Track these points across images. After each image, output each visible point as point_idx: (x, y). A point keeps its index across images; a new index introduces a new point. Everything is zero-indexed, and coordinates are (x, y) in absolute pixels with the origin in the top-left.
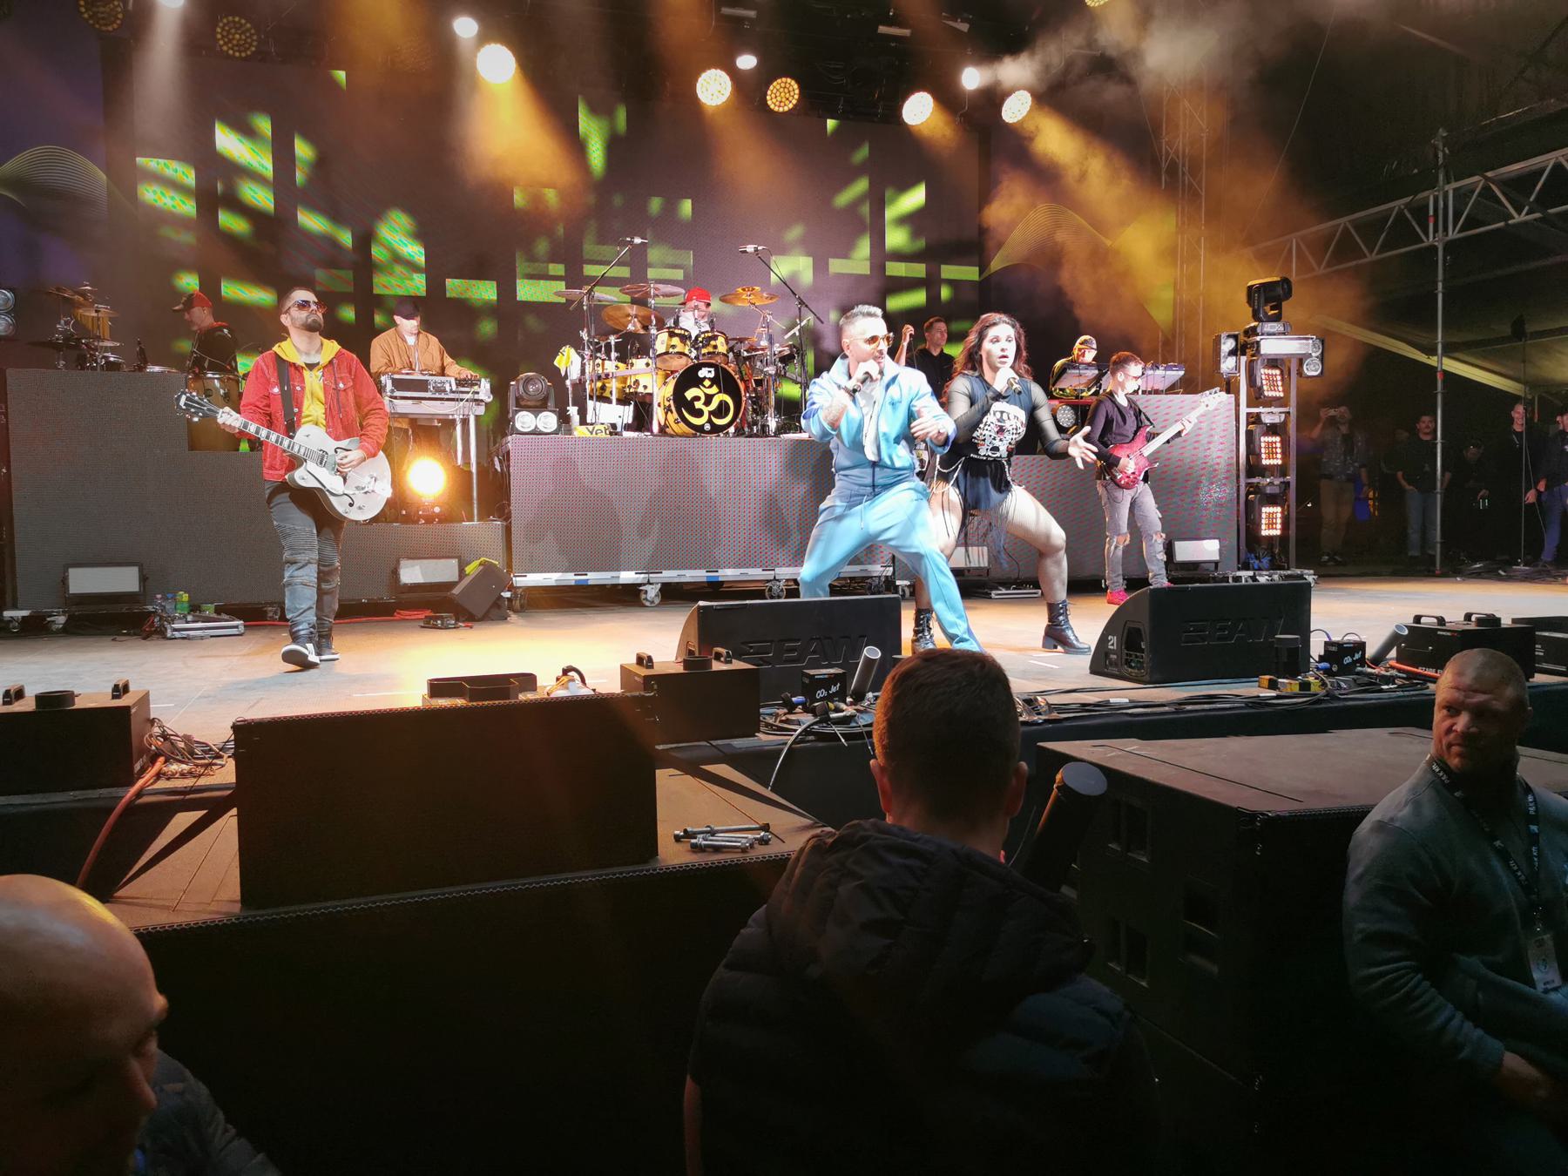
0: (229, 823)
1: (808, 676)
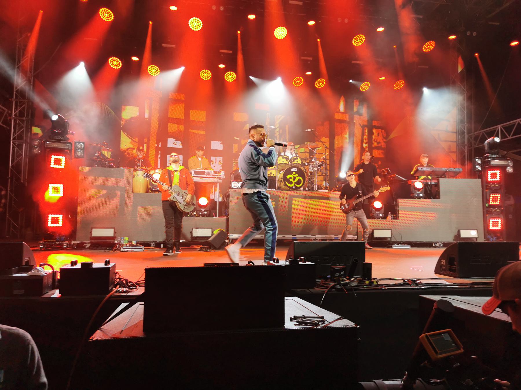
0: (139, 308)
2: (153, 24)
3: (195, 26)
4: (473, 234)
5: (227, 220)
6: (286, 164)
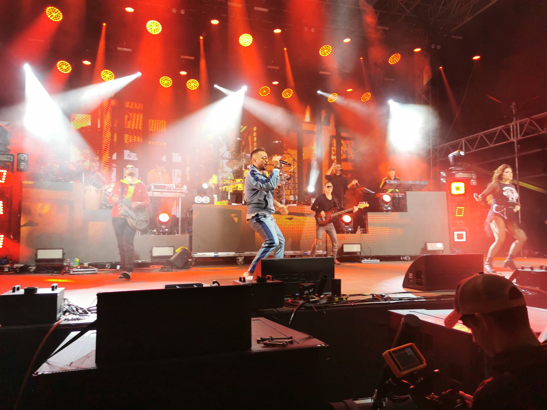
0: (91, 335)
1: (301, 285)
2: (107, 26)
3: (153, 29)
5: (191, 238)
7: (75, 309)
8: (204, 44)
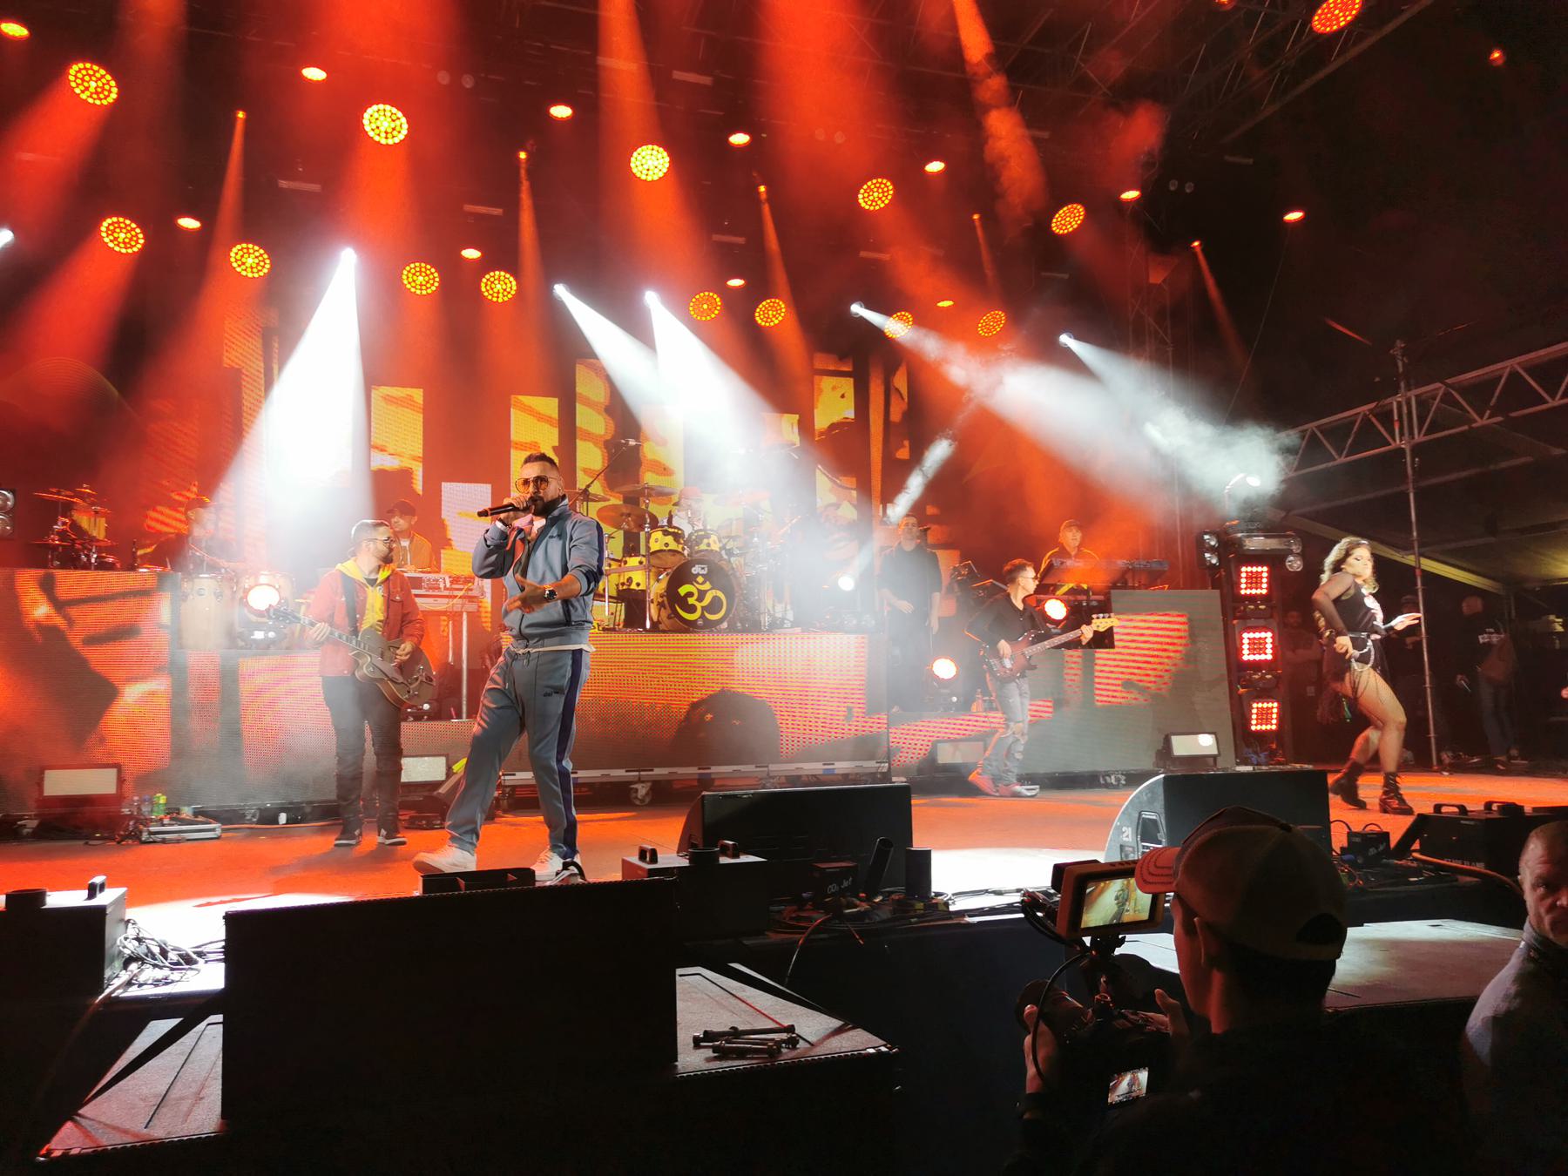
0: (210, 1036)
2: (247, 120)
3: (382, 130)
4: (1205, 743)
6: (674, 552)
7: (156, 950)
8: (528, 172)
